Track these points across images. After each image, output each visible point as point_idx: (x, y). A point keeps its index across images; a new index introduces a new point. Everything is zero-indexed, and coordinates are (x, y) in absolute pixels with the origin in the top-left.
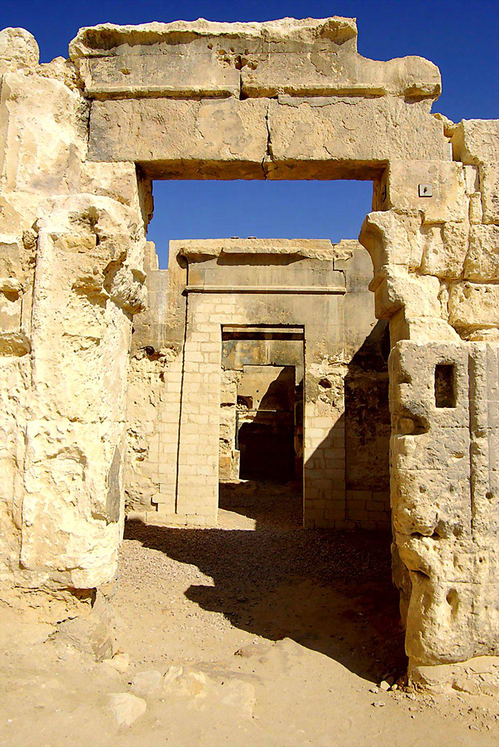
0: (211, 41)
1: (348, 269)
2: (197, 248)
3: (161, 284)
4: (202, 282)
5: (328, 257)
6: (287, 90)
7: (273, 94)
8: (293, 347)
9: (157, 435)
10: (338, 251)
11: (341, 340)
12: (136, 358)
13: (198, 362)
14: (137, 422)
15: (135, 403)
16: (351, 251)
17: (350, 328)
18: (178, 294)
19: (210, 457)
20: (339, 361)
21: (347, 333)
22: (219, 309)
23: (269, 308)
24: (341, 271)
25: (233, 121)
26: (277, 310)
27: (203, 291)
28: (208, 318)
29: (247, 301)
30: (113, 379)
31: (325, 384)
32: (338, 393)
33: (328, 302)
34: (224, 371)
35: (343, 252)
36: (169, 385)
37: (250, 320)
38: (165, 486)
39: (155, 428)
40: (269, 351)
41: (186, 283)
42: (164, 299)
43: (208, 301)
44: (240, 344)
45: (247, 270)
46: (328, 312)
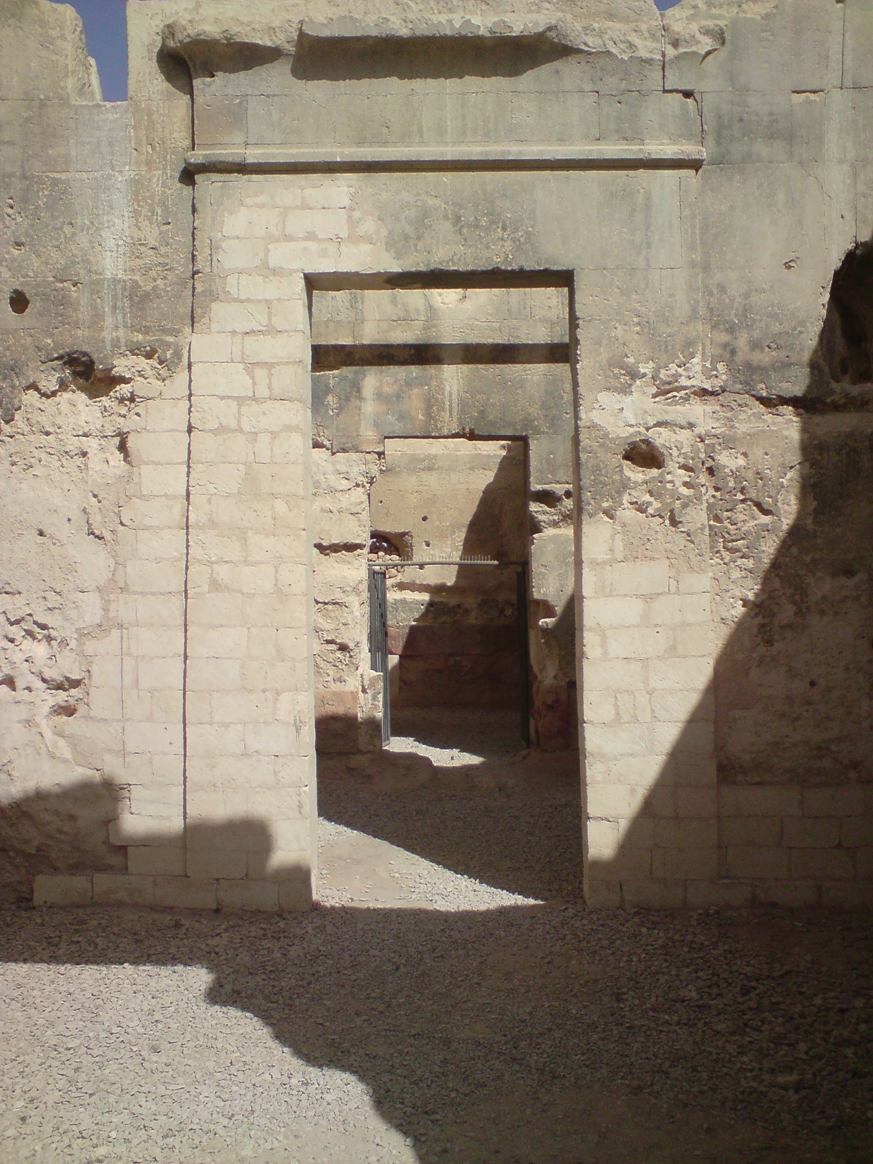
1: (711, 83)
2: (217, 21)
3: (105, 149)
4: (239, 138)
5: (646, 48)
8: (521, 384)
10: (677, 27)
11: (693, 317)
12: (37, 389)
13: (237, 398)
14: (50, 595)
15: (41, 534)
16: (722, 23)
17: (718, 277)
18: (164, 181)
19: (285, 697)
20: (688, 383)
21: (711, 294)
23: (458, 219)
24: (688, 94)
27: (243, 168)
28: (262, 255)
29: (384, 196)
31: (644, 455)
32: (686, 484)
33: (648, 198)
34: (333, 454)
35: (694, 27)
36: (149, 478)
37: (398, 256)
39: (106, 610)
40: (454, 396)
41: (187, 143)
42: (120, 199)
43: (260, 200)
44: (374, 380)
45: (387, 94)
46: (648, 227)
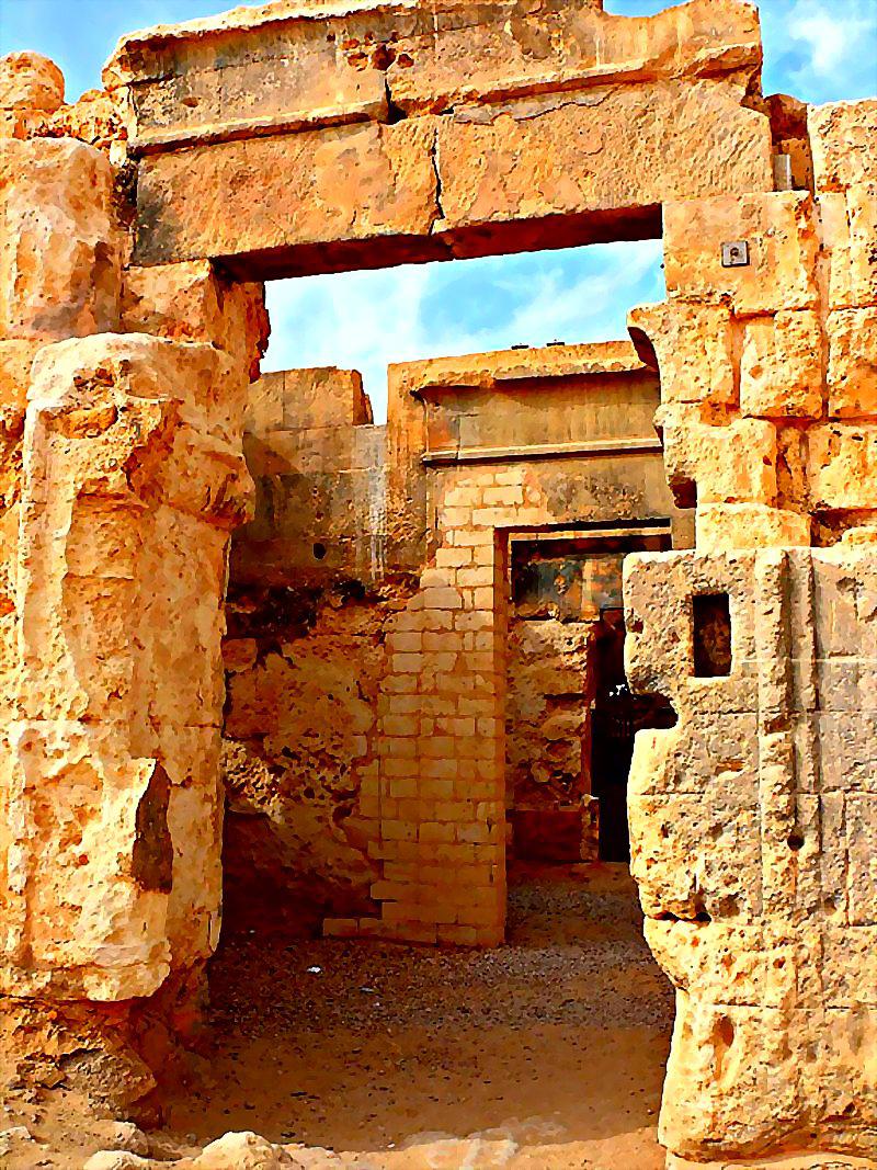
0: (332, 26)
6: (469, 97)
7: (440, 107)
9: (376, 761)
12: (331, 606)
22: (491, 496)
23: (594, 488)
25: (375, 164)
26: (611, 489)
27: (454, 462)
29: (546, 477)
30: (180, 648)
38: (395, 867)
43: (466, 482)
45: (548, 414)
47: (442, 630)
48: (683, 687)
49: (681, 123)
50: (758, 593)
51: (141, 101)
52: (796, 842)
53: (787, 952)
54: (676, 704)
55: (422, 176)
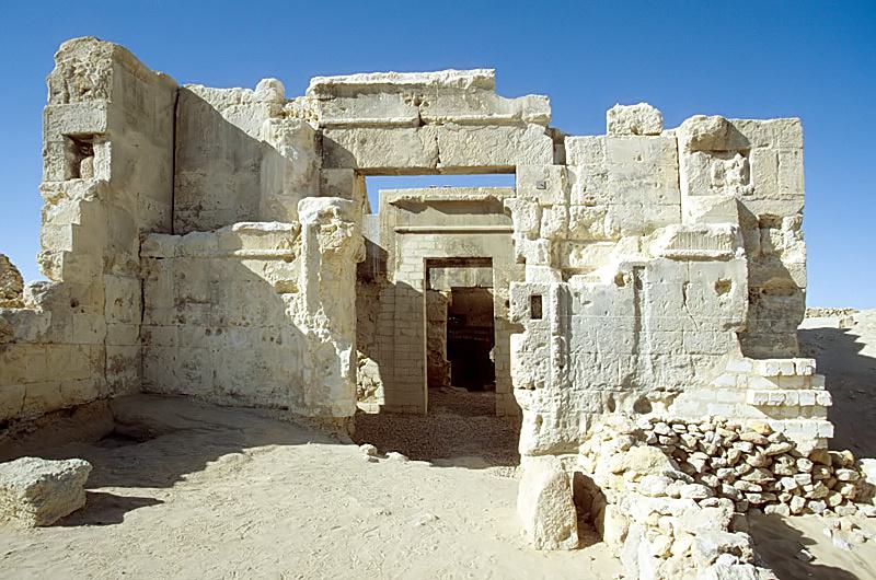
7: (439, 123)
47: (403, 296)
48: (527, 322)
49: (522, 139)
50: (551, 297)
51: (323, 106)
52: (561, 367)
53: (559, 397)
54: (526, 327)
55: (433, 148)
